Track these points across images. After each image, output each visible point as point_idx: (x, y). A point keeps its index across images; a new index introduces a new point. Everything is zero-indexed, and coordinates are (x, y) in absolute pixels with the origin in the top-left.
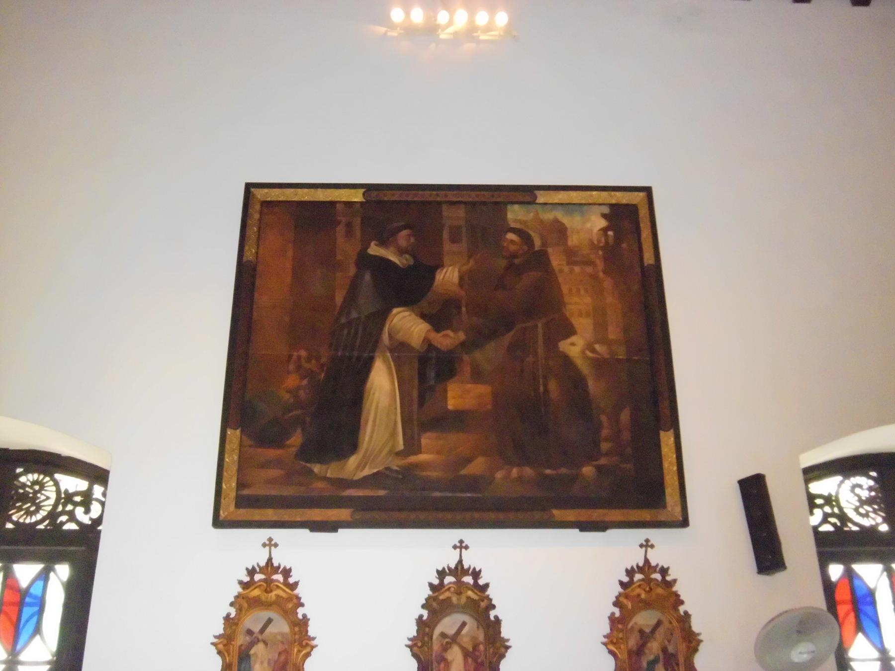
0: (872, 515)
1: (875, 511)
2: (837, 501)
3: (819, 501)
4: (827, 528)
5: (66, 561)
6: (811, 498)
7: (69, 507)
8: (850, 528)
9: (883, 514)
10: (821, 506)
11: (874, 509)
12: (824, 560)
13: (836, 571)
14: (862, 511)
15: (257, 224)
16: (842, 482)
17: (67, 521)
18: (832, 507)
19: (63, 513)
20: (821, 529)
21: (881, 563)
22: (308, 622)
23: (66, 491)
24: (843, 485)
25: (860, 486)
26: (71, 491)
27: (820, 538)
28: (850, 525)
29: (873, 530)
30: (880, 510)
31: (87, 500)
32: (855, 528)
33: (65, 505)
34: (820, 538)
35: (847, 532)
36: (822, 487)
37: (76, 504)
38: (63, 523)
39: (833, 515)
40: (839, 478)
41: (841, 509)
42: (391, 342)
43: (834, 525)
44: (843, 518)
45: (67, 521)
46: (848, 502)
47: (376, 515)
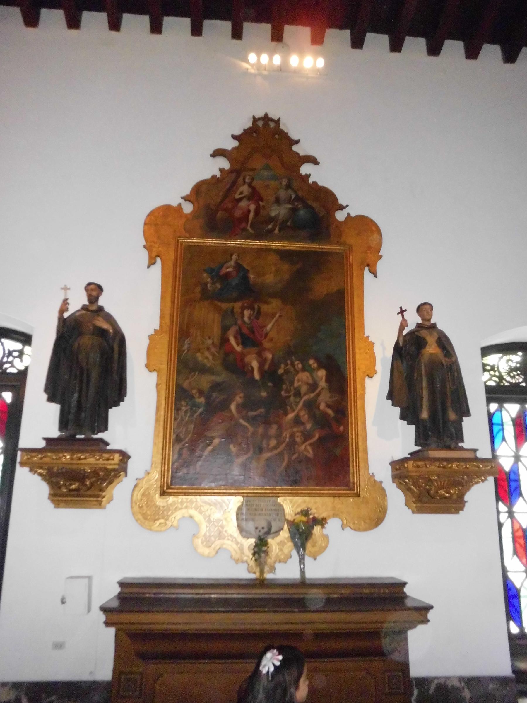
0: (517, 377)
1: (518, 375)
2: (498, 368)
3: (488, 368)
4: (492, 383)
5: (10, 392)
6: (484, 365)
7: (11, 359)
8: (504, 384)
9: (523, 377)
10: (489, 371)
11: (518, 373)
12: (489, 400)
13: (494, 407)
14: (512, 375)
15: (262, 578)
16: (502, 358)
17: (10, 367)
18: (495, 371)
19: (7, 362)
20: (488, 384)
21: (519, 404)
22: (521, 362)
23: (9, 350)
24: (502, 360)
25: (511, 361)
26: (11, 349)
27: (489, 390)
28: (504, 382)
29: (517, 385)
30: (521, 374)
31: (21, 353)
32: (506, 384)
33: (8, 357)
34: (489, 390)
35: (502, 386)
36: (492, 359)
37: (15, 357)
38: (7, 369)
39: (495, 376)
40: (500, 355)
41: (500, 373)
42: (198, 510)
43: (495, 381)
44: (501, 378)
45: (10, 367)
46: (504, 368)
47: (149, 594)
